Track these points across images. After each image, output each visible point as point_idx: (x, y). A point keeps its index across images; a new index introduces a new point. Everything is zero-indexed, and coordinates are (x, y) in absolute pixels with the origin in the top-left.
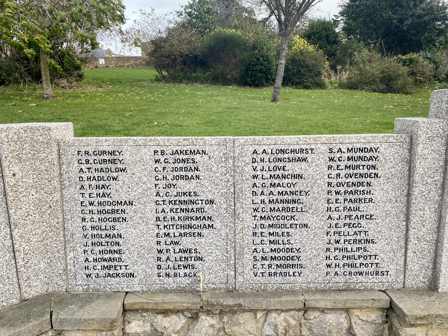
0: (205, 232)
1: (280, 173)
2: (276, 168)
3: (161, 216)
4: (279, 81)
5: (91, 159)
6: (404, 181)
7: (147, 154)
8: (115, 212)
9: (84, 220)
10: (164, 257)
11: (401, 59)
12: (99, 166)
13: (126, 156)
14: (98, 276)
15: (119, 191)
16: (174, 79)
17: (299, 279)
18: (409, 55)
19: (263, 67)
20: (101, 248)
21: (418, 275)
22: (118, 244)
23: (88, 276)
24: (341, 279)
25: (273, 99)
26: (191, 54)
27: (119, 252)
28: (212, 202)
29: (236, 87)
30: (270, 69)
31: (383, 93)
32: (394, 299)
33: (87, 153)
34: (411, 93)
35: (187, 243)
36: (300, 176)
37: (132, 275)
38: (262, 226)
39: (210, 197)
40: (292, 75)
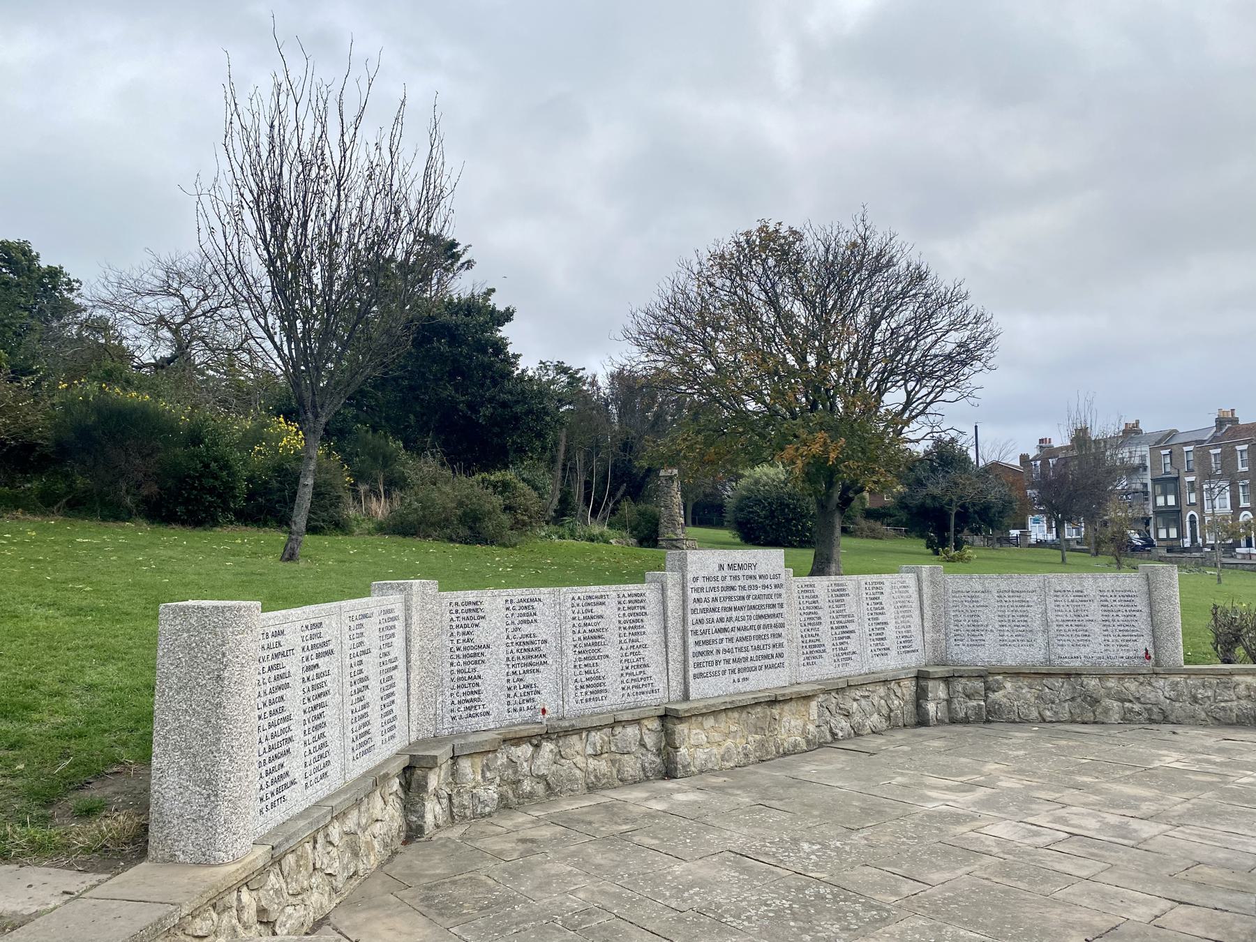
0: (541, 668)
1: (589, 614)
2: (587, 611)
3: (510, 656)
4: (300, 519)
5: (460, 608)
6: (661, 617)
7: (500, 602)
8: (475, 655)
9: (452, 664)
10: (512, 694)
11: (490, 482)
12: (465, 615)
13: (485, 606)
14: (461, 718)
15: (479, 637)
17: (606, 702)
18: (498, 474)
19: (217, 483)
20: (464, 690)
21: (676, 693)
22: (478, 685)
23: (453, 718)
24: (632, 699)
27: (478, 692)
28: (545, 642)
30: (234, 488)
33: (457, 604)
35: (529, 678)
36: (601, 617)
37: (488, 713)
38: (580, 659)
39: (545, 637)
40: (278, 502)
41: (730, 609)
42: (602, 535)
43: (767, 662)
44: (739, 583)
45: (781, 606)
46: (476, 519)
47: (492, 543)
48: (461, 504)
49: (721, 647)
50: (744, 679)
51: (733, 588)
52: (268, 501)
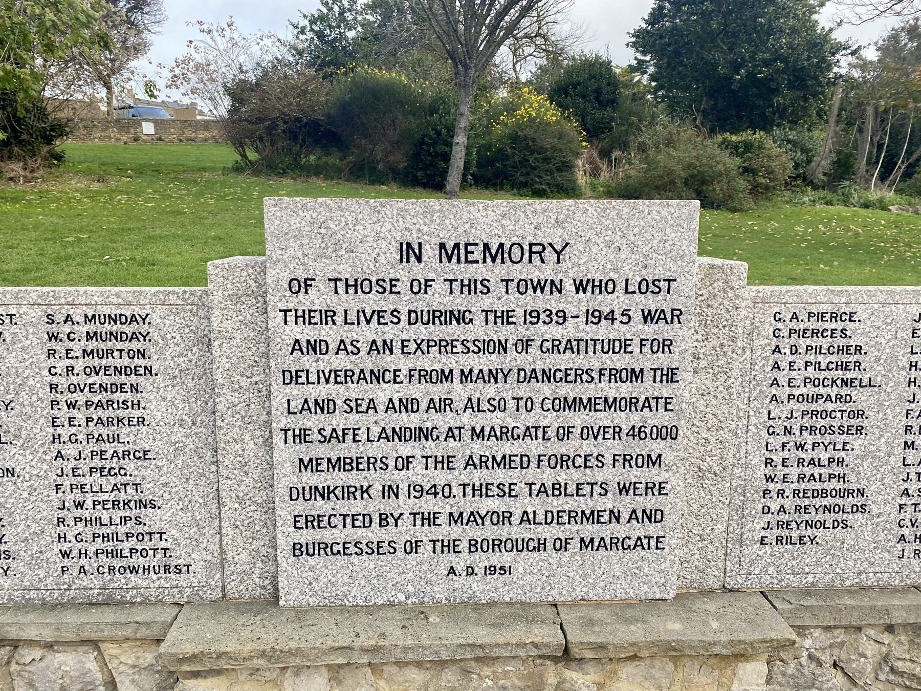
29: (394, 188)
34: (741, 210)
41: (446, 376)
42: (881, 201)
43: (588, 530)
44: (487, 302)
45: (671, 375)
46: (704, 182)
47: (718, 208)
48: (690, 166)
49: (401, 478)
50: (491, 570)
51: (460, 317)
52: (505, 166)
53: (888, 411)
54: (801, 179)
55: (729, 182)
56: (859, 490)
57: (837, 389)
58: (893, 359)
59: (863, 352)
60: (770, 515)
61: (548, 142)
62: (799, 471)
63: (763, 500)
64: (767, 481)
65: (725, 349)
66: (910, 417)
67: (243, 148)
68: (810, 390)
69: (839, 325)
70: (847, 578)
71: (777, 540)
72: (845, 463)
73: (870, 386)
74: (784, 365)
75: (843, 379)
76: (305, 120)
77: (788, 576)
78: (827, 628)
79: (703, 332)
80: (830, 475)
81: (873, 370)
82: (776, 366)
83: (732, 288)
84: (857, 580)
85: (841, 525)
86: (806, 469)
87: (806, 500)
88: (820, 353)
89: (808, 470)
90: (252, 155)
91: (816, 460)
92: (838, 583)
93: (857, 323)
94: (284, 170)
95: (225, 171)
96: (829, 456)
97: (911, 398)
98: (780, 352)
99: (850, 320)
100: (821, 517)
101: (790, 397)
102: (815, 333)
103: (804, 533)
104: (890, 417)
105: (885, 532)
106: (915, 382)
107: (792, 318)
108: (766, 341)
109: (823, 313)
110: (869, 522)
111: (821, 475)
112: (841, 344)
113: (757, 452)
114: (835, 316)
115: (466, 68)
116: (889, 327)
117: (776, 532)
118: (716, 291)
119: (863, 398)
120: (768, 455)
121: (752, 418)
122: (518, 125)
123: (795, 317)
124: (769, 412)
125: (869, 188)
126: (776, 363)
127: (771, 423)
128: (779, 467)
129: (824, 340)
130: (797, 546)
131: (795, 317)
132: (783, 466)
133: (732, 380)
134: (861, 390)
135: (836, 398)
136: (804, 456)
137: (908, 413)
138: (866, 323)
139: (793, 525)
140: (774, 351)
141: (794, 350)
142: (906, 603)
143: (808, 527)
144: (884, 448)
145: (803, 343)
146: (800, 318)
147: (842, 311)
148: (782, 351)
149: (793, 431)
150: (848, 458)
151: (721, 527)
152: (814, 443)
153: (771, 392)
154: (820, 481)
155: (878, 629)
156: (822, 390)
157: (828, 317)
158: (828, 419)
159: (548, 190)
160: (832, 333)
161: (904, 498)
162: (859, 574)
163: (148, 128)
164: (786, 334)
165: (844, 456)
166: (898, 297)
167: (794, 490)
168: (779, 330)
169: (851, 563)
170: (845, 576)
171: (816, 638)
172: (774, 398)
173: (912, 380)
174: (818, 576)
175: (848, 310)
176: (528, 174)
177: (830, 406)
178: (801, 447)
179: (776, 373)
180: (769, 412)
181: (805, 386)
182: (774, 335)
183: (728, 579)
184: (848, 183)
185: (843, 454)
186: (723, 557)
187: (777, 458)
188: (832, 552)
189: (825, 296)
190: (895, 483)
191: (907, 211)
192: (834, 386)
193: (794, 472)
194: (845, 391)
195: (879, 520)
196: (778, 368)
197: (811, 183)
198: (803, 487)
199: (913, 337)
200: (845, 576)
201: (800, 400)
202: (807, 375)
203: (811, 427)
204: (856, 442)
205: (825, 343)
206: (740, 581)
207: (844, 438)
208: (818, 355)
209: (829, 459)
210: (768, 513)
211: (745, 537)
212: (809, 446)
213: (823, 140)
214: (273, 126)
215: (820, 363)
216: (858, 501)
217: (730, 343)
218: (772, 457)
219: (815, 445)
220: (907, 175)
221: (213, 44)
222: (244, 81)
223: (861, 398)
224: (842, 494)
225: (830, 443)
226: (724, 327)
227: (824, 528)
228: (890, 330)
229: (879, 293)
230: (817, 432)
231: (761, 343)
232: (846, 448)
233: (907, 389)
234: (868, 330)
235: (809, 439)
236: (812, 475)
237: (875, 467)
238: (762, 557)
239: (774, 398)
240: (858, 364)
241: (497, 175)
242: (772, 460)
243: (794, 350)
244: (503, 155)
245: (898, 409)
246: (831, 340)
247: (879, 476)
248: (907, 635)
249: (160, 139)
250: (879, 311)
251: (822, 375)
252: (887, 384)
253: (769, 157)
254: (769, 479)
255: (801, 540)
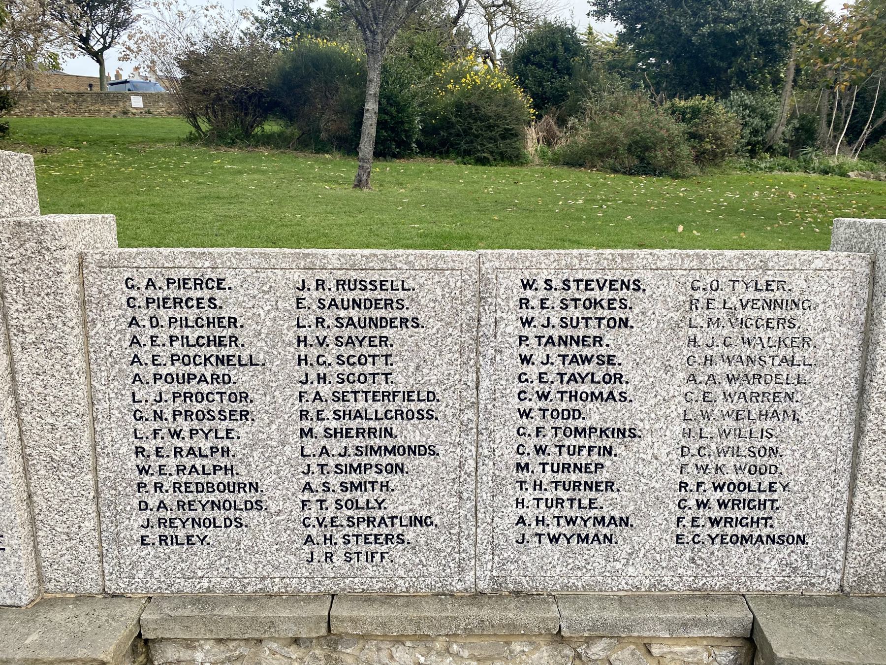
4: (366, 146)
16: (219, 138)
25: (356, 183)
26: (252, 88)
29: (338, 156)
31: (631, 174)
32: (761, 620)
34: (683, 177)
42: (840, 167)
46: (647, 149)
47: (660, 175)
53: (277, 393)
54: (756, 147)
55: (673, 147)
56: (251, 484)
57: (212, 368)
58: (275, 334)
59: (238, 325)
60: (148, 511)
61: (489, 110)
62: (177, 462)
63: (138, 495)
64: (141, 473)
65: (54, 321)
66: (304, 400)
67: (195, 118)
68: (179, 369)
69: (206, 294)
70: (249, 584)
71: (161, 540)
72: (231, 453)
73: (252, 364)
74: (145, 339)
75: (217, 356)
76: (252, 91)
77: (179, 581)
78: (220, 641)
79: (23, 301)
80: (215, 466)
81: (252, 345)
82: (135, 341)
83: (48, 250)
84: (261, 586)
85: (234, 523)
86: (184, 460)
87: (190, 495)
88: (187, 326)
89: (188, 462)
90: (205, 126)
91: (196, 450)
92: (238, 588)
93: (228, 291)
94: (233, 140)
95: (180, 142)
96: (211, 445)
97: (303, 378)
98: (137, 324)
99: (219, 288)
100: (209, 514)
101: (157, 377)
102: (177, 302)
103: (191, 532)
104: (280, 400)
105: (288, 532)
106: (306, 360)
107: (148, 285)
108: (120, 312)
109: (184, 280)
110: (267, 520)
111: (203, 466)
112: (211, 316)
113: (125, 440)
114: (200, 283)
115: (374, 33)
116: (267, 296)
117: (158, 530)
118: (29, 253)
119: (244, 379)
120: (137, 443)
121: (113, 401)
122: (465, 94)
123: (151, 283)
124: (133, 394)
125: (834, 153)
126: (135, 337)
127: (137, 406)
128: (153, 457)
129: (189, 311)
130: (185, 547)
131: (151, 283)
132: (157, 456)
133: (70, 357)
134: (241, 369)
135: (212, 378)
136: (180, 444)
137: (301, 396)
138: (238, 292)
139: (178, 523)
140: (131, 324)
141: (154, 322)
142: (297, 613)
143: (196, 526)
144: (275, 436)
145: (164, 315)
146: (158, 285)
147: (207, 277)
148: (141, 323)
149: (164, 417)
150: (235, 447)
151: (89, 525)
152: (191, 430)
153: (133, 372)
154: (204, 473)
155: (281, 642)
156: (193, 369)
157: (191, 284)
158: (205, 402)
159: (491, 158)
160: (198, 303)
161: (306, 493)
162: (263, 579)
163: (137, 102)
164: (143, 304)
165: (230, 445)
166: (273, 260)
167: (175, 483)
168: (134, 299)
169: (251, 567)
170: (246, 581)
171: (208, 651)
172: (137, 378)
173: (303, 357)
174: (213, 580)
175: (214, 276)
176: (472, 142)
177: (205, 388)
178: (177, 434)
179: (136, 349)
180: (133, 394)
181: (173, 364)
182: (129, 305)
183: (108, 583)
184: (810, 149)
185: (227, 443)
186: (97, 559)
187: (149, 446)
188: (227, 554)
189: (184, 259)
190: (293, 476)
191: (869, 177)
192: (208, 364)
193: (172, 463)
194: (221, 370)
195: (278, 518)
196: (138, 342)
197: (770, 150)
198: (184, 480)
199: (298, 308)
200: (246, 581)
201: (169, 380)
202: (173, 352)
203: (186, 411)
204: (242, 429)
205: (192, 314)
206: (123, 586)
207: (226, 424)
208: (184, 329)
209: (212, 448)
210: (146, 509)
211: (122, 535)
212: (185, 434)
213: (785, 106)
214: (219, 99)
215: (187, 337)
216: (253, 496)
217: (59, 313)
218: (143, 445)
219: (192, 432)
220: (874, 137)
221: (160, 17)
222: (192, 52)
223: (242, 378)
224: (231, 489)
225: (211, 430)
226: (48, 294)
227: (215, 526)
228: (268, 300)
229: (250, 257)
230: (194, 417)
231: (114, 314)
232: (230, 436)
233: (297, 367)
234: (241, 299)
235: (185, 426)
236: (193, 466)
237: (268, 457)
238: (145, 559)
239: (137, 378)
240: (234, 339)
241: (444, 142)
242: (144, 450)
243: (154, 322)
244: (448, 123)
245: (288, 392)
246: (197, 311)
247: (273, 468)
248: (323, 649)
249: (149, 113)
250: (823, 278)
251: (192, 352)
252: (272, 362)
253: (717, 122)
254: (142, 470)
255: (188, 540)
